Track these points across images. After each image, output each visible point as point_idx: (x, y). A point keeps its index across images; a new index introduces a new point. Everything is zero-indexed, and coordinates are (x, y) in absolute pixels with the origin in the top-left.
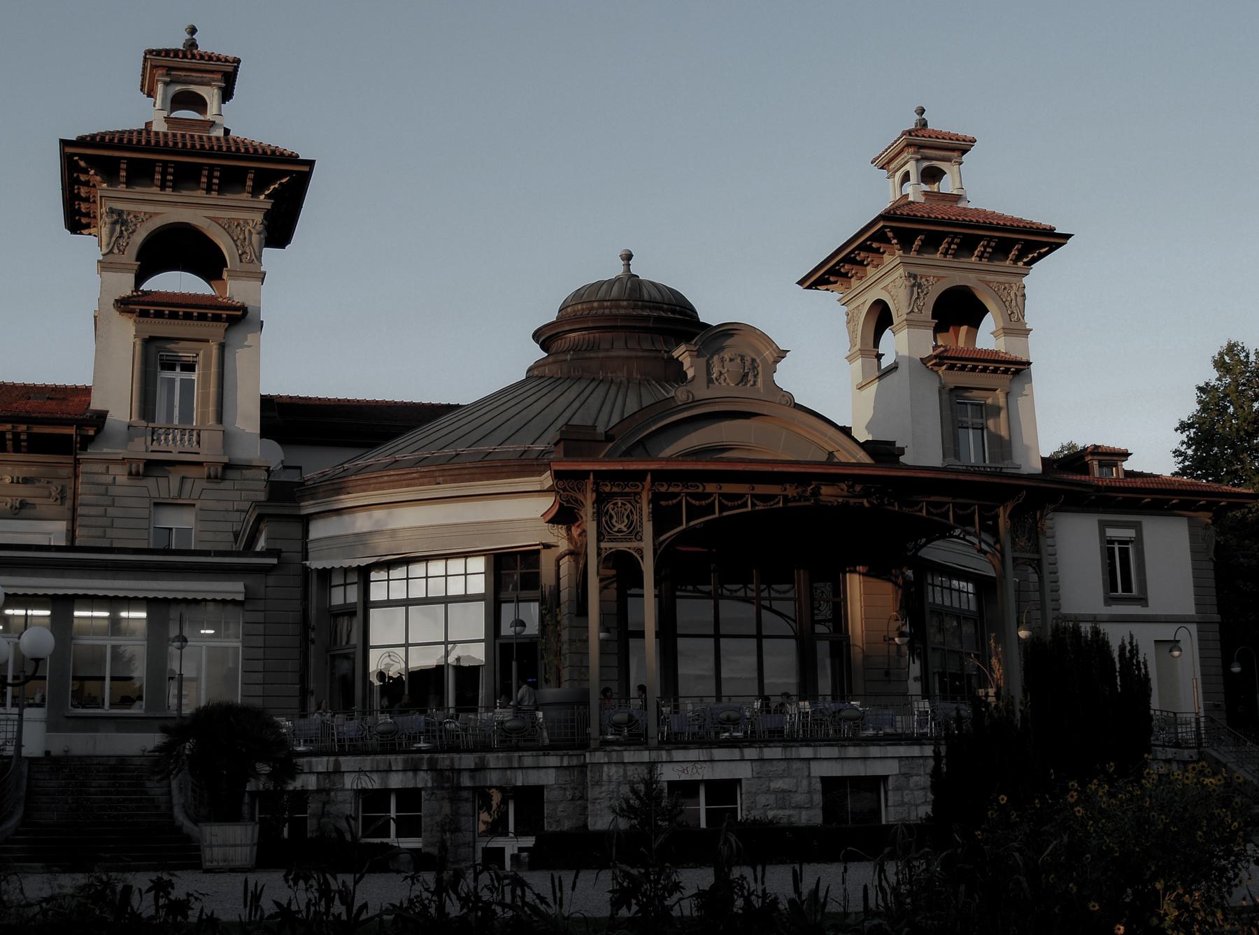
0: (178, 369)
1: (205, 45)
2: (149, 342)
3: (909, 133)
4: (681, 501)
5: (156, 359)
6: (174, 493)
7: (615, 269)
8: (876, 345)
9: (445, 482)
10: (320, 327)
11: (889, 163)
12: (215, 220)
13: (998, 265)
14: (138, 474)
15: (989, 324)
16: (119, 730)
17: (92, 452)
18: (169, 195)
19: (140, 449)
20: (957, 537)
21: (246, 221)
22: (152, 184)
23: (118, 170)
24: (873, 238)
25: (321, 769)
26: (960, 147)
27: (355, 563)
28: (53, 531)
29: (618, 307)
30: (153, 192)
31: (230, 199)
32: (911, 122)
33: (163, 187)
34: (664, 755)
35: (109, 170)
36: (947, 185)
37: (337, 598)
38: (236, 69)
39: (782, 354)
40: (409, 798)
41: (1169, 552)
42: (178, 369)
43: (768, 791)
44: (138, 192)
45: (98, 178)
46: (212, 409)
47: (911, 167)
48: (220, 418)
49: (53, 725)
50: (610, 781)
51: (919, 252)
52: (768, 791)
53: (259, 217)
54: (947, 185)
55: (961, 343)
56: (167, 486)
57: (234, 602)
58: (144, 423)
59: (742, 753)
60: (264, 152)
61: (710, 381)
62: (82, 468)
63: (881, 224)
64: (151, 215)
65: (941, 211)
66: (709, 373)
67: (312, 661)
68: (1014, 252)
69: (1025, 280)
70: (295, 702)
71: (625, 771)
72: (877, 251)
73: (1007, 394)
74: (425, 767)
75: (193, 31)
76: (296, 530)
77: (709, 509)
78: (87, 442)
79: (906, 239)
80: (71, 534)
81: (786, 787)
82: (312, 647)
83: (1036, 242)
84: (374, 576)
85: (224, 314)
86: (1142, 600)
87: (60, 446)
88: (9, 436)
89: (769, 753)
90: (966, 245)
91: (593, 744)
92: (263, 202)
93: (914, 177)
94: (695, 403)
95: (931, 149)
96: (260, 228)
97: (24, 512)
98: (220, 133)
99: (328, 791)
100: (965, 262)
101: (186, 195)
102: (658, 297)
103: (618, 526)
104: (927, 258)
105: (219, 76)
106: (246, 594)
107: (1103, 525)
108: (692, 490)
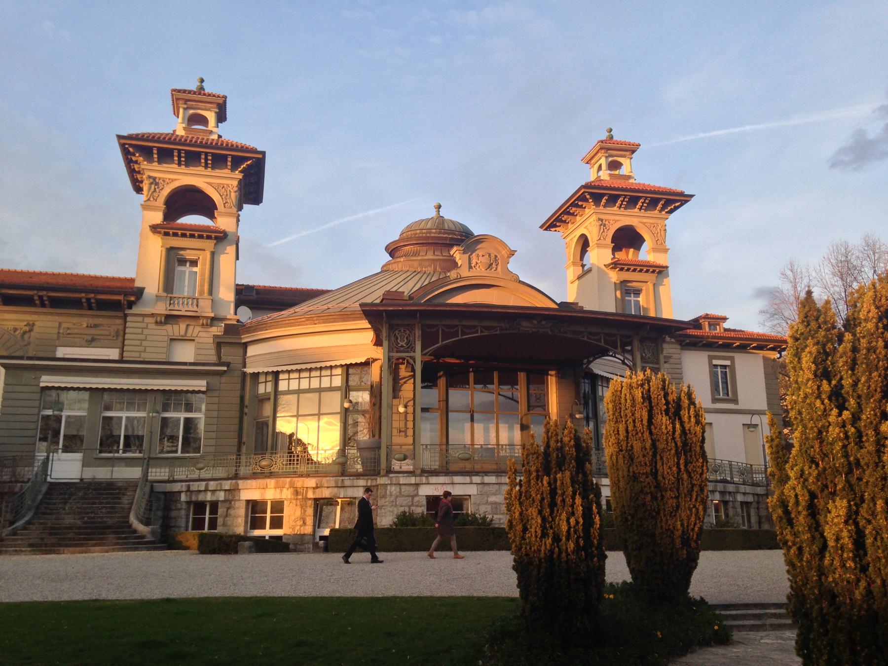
0: (188, 264)
1: (209, 88)
2: (171, 251)
3: (602, 142)
4: (438, 330)
5: (174, 260)
6: (182, 333)
7: (432, 214)
8: (582, 259)
9: (319, 323)
10: (270, 244)
11: (591, 160)
12: (210, 184)
13: (650, 213)
14: (161, 322)
15: (645, 247)
16: (127, 466)
17: (135, 310)
18: (183, 169)
19: (161, 309)
20: (611, 356)
21: (228, 185)
22: (172, 162)
23: (152, 154)
24: (577, 199)
25: (227, 487)
26: (631, 149)
27: (270, 370)
28: (113, 354)
29: (430, 233)
30: (174, 167)
31: (218, 172)
32: (604, 136)
33: (179, 164)
34: (424, 480)
35: (147, 152)
36: (624, 171)
37: (261, 389)
38: (225, 102)
39: (512, 253)
40: (278, 507)
41: (750, 373)
42: (188, 264)
43: (487, 503)
44: (165, 167)
45: (141, 158)
46: (206, 287)
47: (603, 161)
48: (211, 293)
49: (85, 464)
50: (391, 495)
51: (605, 206)
52: (487, 503)
53: (235, 183)
54: (624, 171)
55: (630, 256)
56: (180, 329)
57: (199, 392)
58: (165, 294)
59: (471, 480)
60: (232, 145)
61: (470, 267)
62: (129, 319)
63: (583, 191)
64: (173, 180)
65: (617, 183)
66: (470, 263)
67: (245, 425)
68: (660, 206)
69: (667, 222)
70: (235, 449)
71: (400, 489)
72: (581, 207)
73: (654, 284)
74: (287, 486)
75: (202, 81)
76: (240, 351)
77: (455, 334)
78: (130, 305)
79: (597, 199)
80: (122, 354)
81: (497, 500)
82: (245, 418)
83: (670, 201)
84: (281, 376)
85: (213, 235)
86: (735, 401)
87: (115, 306)
88: (84, 300)
89: (487, 479)
90: (632, 202)
91: (382, 472)
92: (238, 175)
93: (604, 167)
94: (461, 279)
95: (614, 150)
96: (236, 189)
97: (93, 344)
98: (215, 137)
99: (230, 501)
100: (630, 212)
101: (192, 170)
102: (453, 228)
103: (401, 343)
104: (609, 210)
105: (215, 106)
106: (207, 387)
107: (711, 358)
108: (444, 323)
